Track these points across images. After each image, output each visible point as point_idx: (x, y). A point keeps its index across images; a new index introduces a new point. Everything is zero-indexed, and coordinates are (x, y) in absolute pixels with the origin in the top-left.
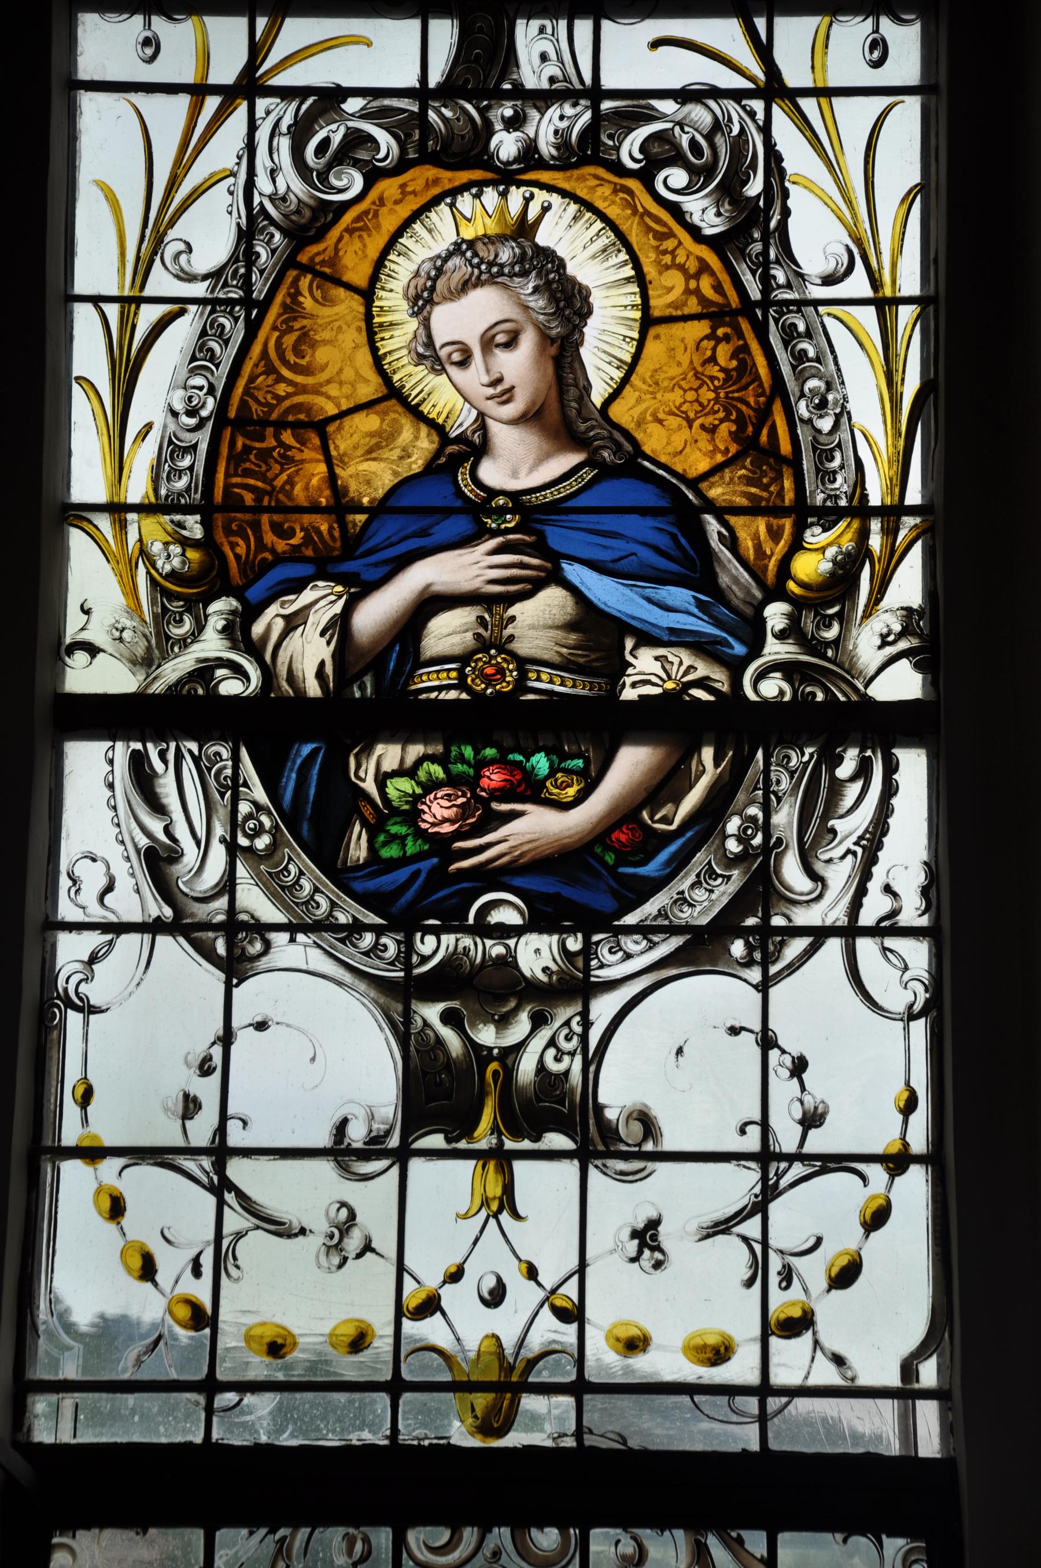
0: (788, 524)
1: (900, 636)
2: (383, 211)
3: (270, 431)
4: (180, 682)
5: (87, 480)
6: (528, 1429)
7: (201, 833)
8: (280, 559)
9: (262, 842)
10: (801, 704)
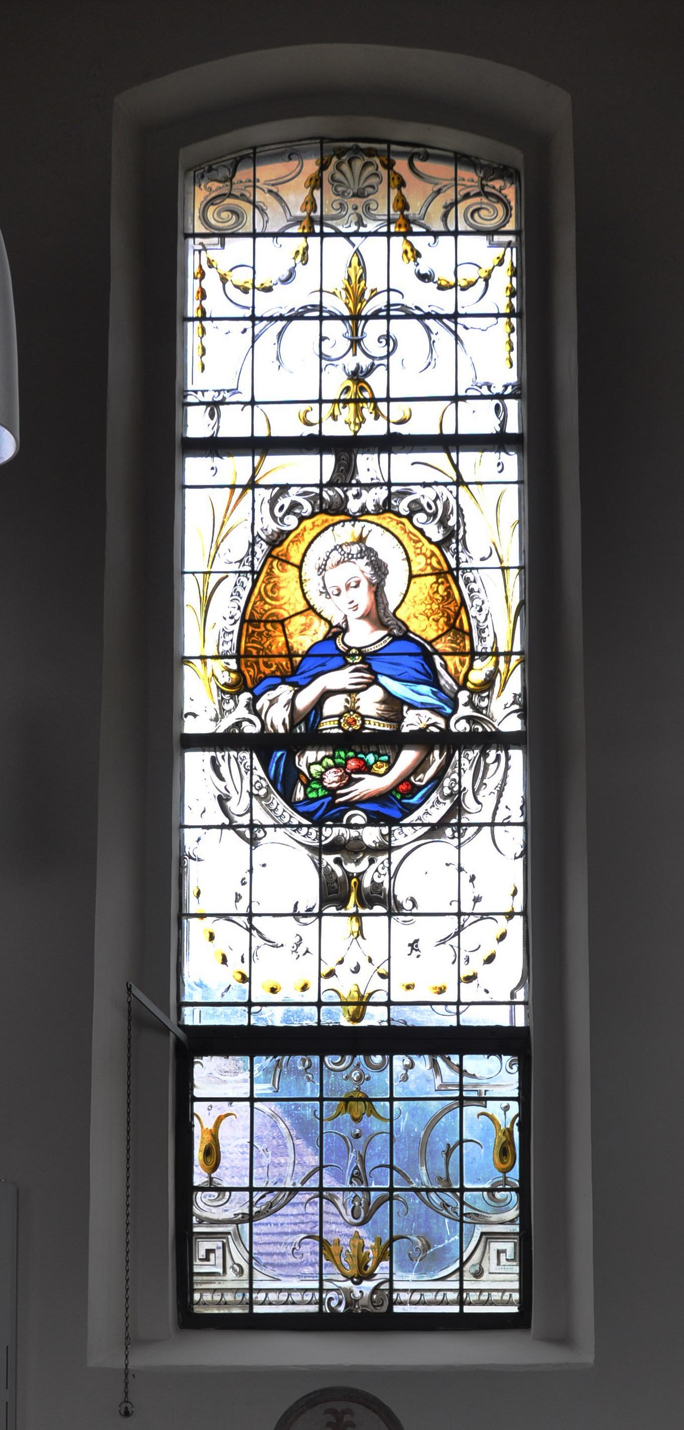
0: (467, 659)
1: (513, 703)
2: (306, 533)
3: (262, 624)
4: (229, 728)
5: (191, 644)
6: (369, 1019)
7: (239, 790)
8: (266, 677)
9: (262, 792)
10: (473, 733)
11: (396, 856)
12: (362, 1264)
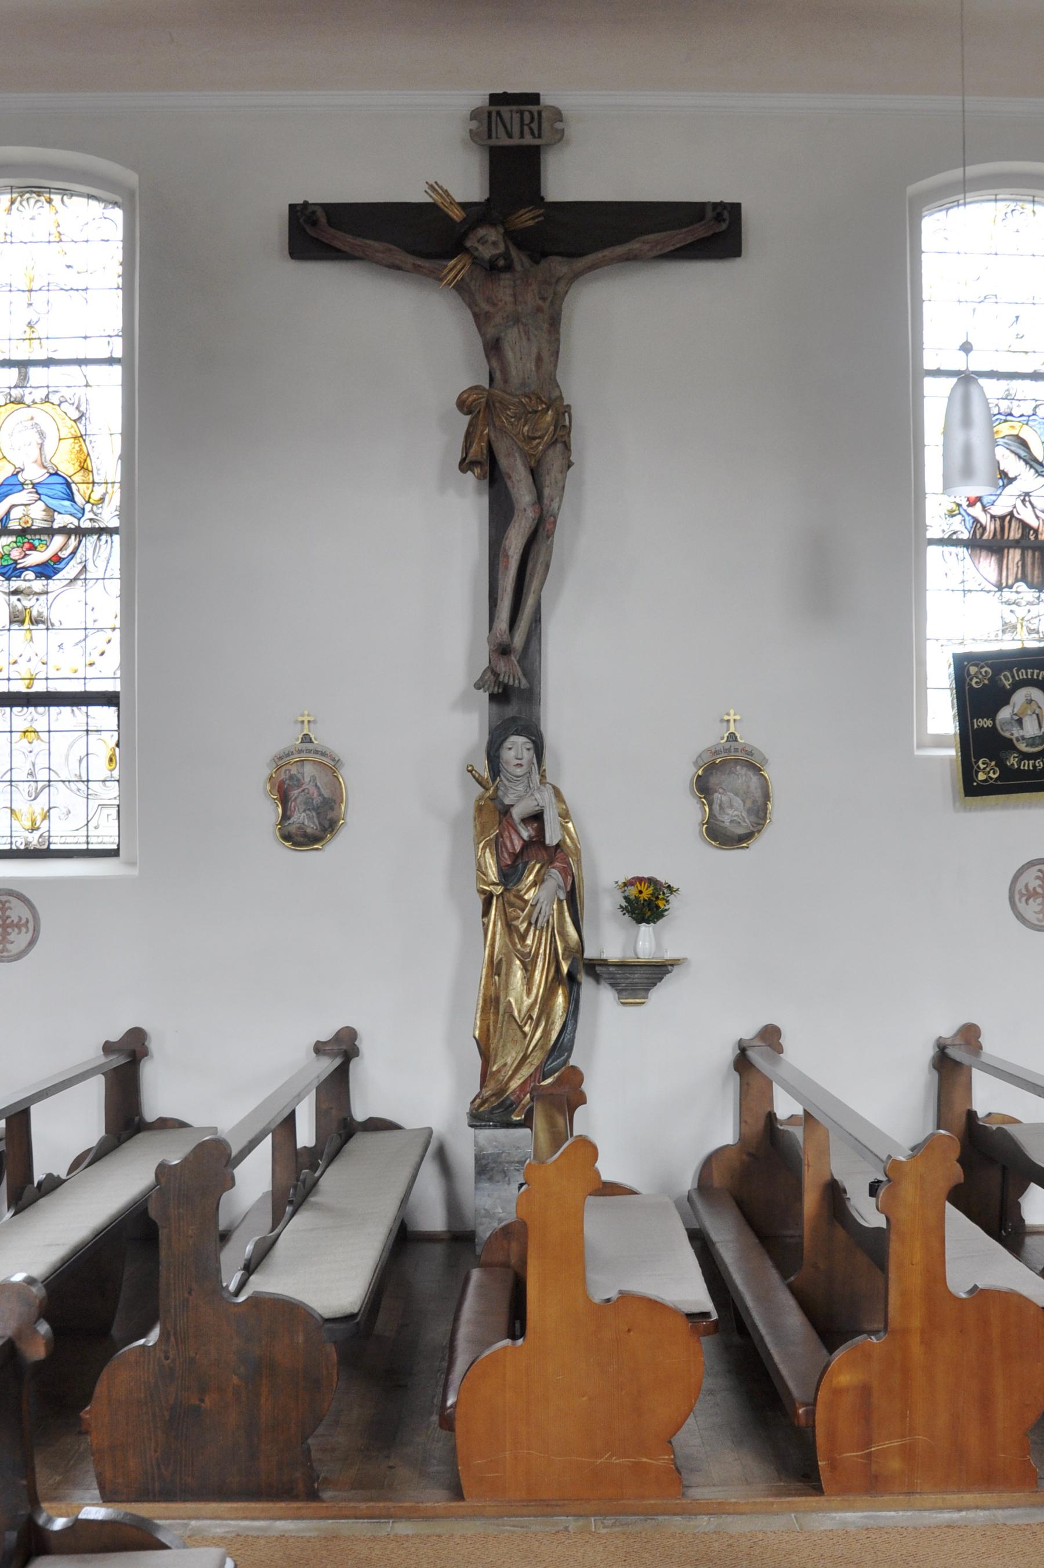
11: (51, 596)
12: (34, 822)
